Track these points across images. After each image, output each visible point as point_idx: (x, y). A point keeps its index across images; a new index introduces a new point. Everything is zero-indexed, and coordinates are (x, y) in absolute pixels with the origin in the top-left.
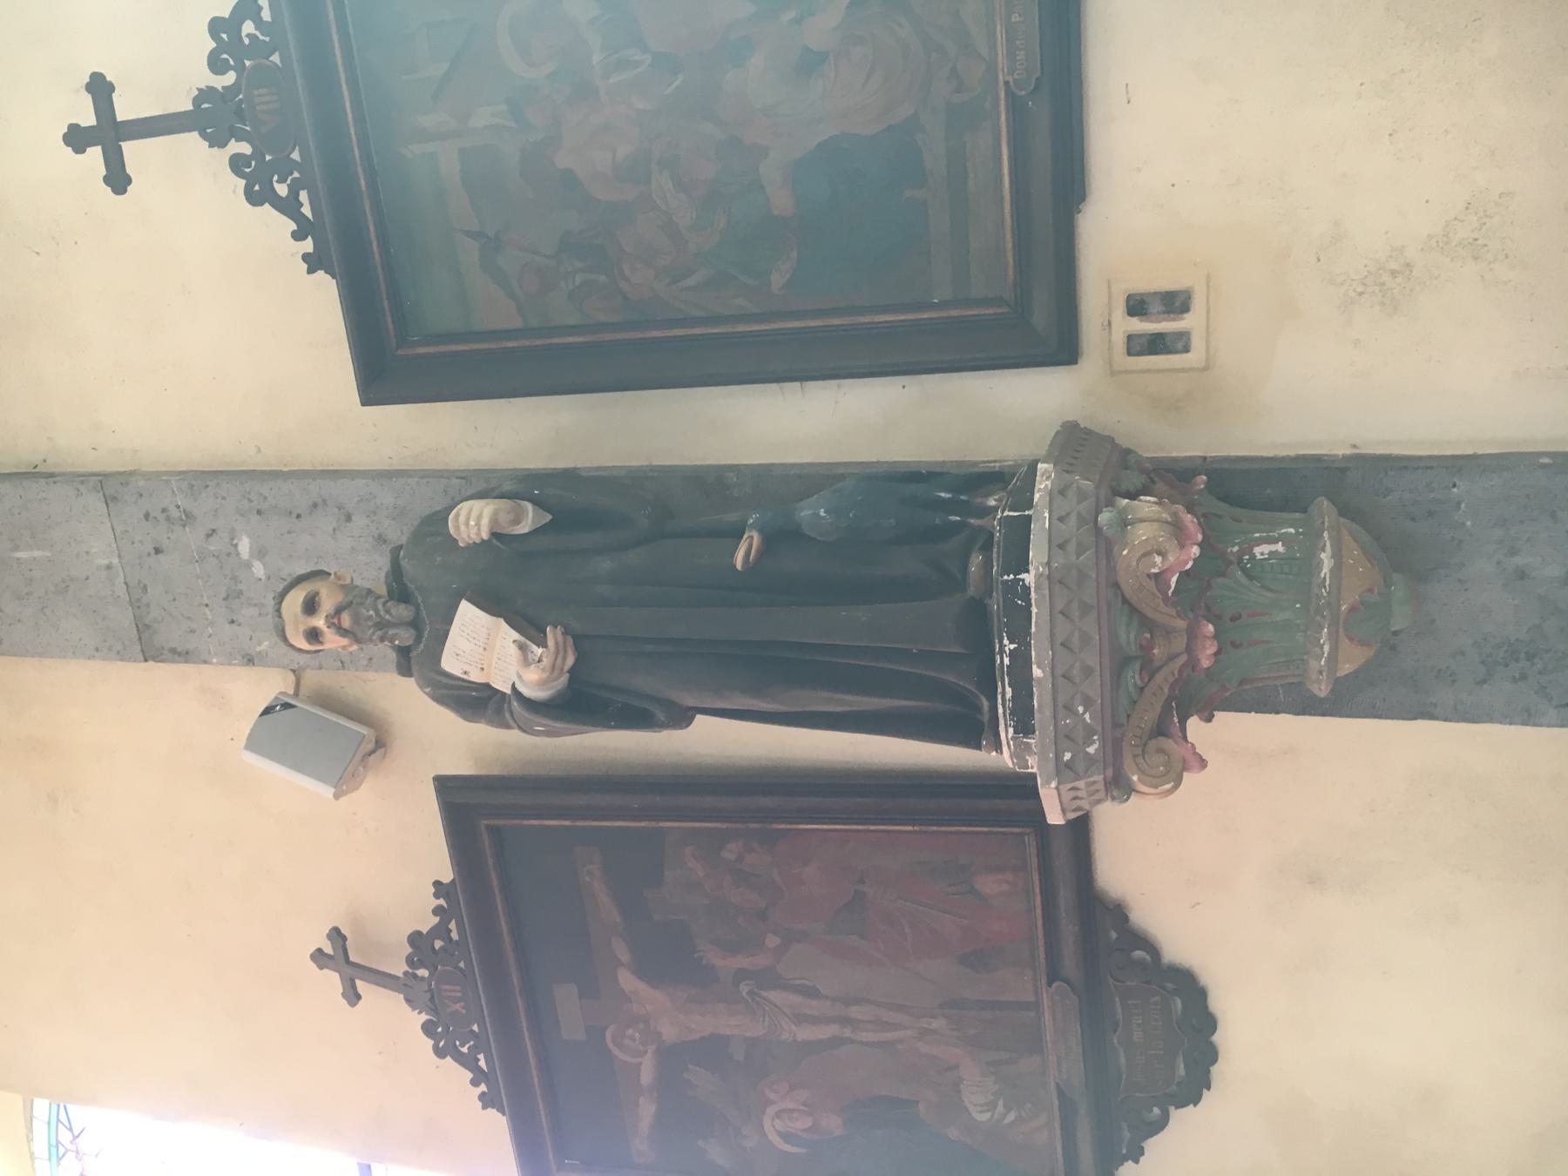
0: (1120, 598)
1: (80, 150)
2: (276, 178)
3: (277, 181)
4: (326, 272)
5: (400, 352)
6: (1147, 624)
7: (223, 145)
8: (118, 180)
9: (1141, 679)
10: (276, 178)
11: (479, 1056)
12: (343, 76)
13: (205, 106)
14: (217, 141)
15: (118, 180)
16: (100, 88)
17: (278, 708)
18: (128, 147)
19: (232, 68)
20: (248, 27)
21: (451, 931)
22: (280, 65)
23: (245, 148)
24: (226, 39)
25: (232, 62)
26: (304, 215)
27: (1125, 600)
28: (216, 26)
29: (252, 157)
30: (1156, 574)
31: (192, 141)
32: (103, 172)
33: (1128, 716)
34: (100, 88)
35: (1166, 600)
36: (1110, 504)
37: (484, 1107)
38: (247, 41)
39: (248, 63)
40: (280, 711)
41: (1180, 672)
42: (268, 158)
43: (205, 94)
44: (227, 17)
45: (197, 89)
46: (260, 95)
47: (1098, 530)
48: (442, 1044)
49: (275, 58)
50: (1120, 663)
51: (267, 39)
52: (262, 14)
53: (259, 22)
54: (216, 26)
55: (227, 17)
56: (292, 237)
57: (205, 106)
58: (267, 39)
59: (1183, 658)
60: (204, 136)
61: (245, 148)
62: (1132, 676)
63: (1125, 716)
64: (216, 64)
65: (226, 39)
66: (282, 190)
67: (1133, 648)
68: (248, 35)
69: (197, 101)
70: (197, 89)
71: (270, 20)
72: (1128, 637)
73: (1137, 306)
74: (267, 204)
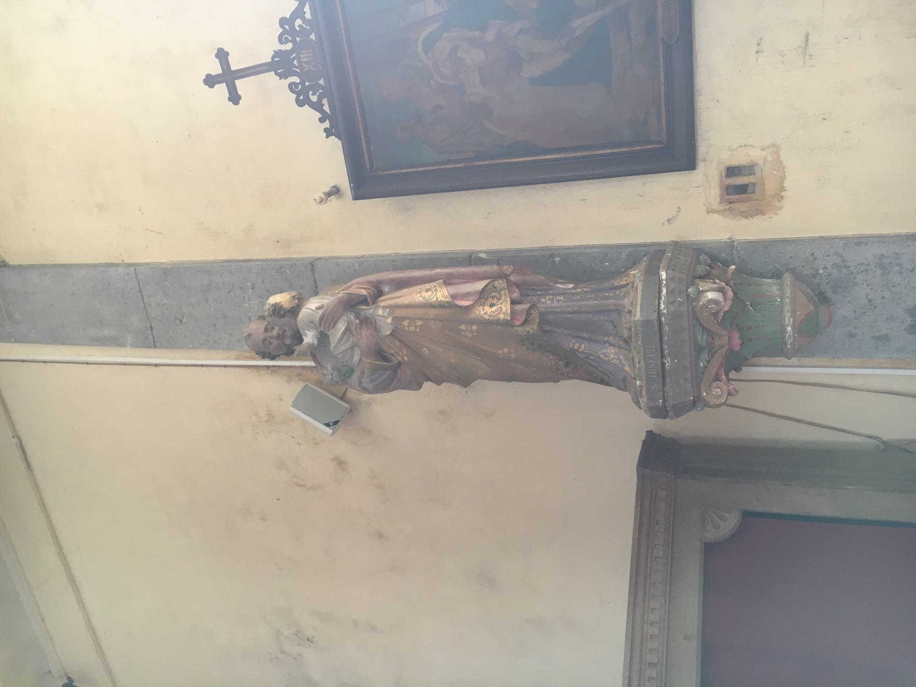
0: (698, 324)
1: (212, 86)
2: (311, 92)
3: (312, 95)
4: (336, 137)
5: (371, 174)
6: (711, 334)
7: (286, 78)
8: (235, 98)
9: (708, 357)
10: (311, 92)
11: (327, 122)
12: (363, 137)
13: (276, 59)
14: (282, 76)
15: (235, 98)
16: (222, 55)
17: (331, 424)
18: (237, 82)
19: (290, 41)
20: (298, 22)
21: (324, 105)
22: (315, 40)
23: (296, 79)
24: (288, 28)
25: (290, 38)
26: (325, 111)
27: (701, 325)
28: (283, 21)
29: (300, 84)
30: (714, 313)
31: (271, 78)
32: (228, 96)
33: (703, 373)
34: (222, 55)
35: (718, 323)
36: (692, 284)
37: (327, 137)
38: (298, 29)
39: (298, 39)
40: (332, 425)
41: (726, 353)
42: (307, 84)
43: (277, 53)
44: (288, 17)
45: (274, 51)
46: (304, 58)
47: (688, 296)
48: (301, 97)
49: (313, 37)
50: (699, 350)
51: (308, 28)
52: (306, 15)
53: (304, 19)
54: (283, 21)
55: (288, 17)
56: (319, 120)
57: (276, 59)
58: (308, 28)
59: (728, 346)
60: (277, 74)
61: (296, 79)
62: (704, 356)
63: (702, 373)
64: (281, 40)
65: (288, 28)
66: (314, 98)
67: (704, 342)
68: (299, 26)
69: (273, 58)
70: (274, 51)
71: (310, 18)
72: (702, 339)
73: (732, 171)
74: (306, 105)
